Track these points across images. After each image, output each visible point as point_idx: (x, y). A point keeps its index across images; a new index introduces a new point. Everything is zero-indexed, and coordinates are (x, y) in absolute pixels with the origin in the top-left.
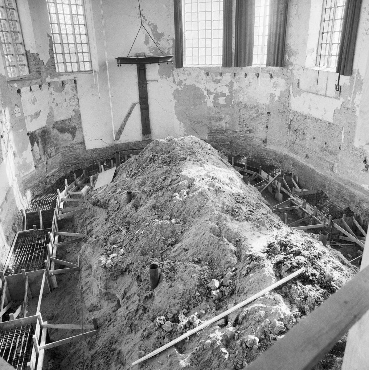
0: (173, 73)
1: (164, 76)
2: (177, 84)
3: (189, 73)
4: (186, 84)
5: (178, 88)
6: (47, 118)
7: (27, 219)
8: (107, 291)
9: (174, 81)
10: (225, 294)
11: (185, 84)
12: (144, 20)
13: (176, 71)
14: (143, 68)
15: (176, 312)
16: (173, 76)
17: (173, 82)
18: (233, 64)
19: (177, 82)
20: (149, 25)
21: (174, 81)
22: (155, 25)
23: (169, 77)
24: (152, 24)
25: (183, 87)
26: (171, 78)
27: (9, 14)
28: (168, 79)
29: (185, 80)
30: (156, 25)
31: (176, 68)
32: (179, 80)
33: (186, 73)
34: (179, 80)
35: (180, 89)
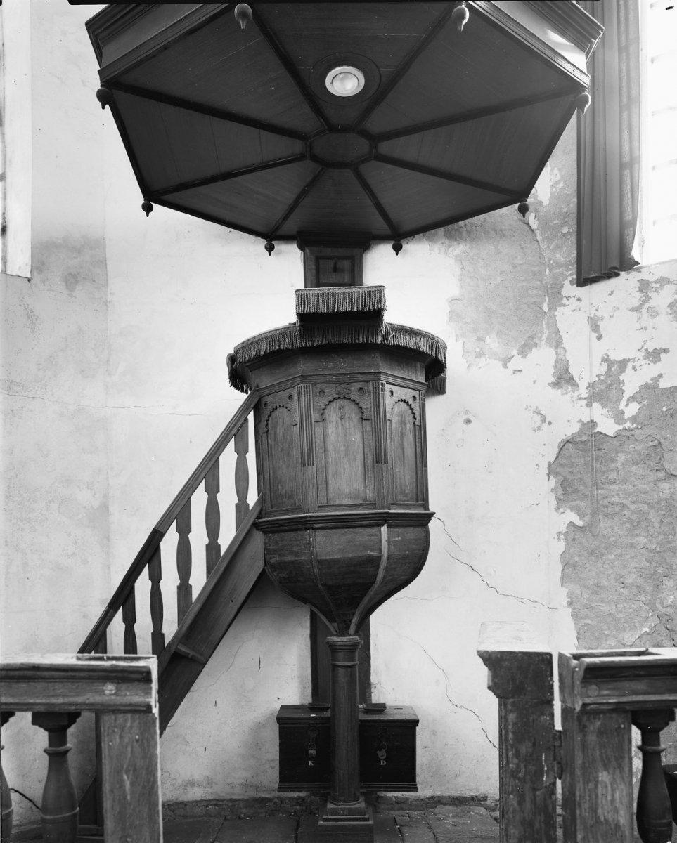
1: (493, 343)
2: (583, 391)
4: (663, 384)
5: (592, 424)
7: (551, 687)
8: (547, 422)
9: (563, 379)
10: (275, 434)
15: (421, 552)
16: (557, 343)
17: (556, 385)
18: (101, 838)
21: (563, 379)
23: (524, 350)
25: (632, 410)
26: (543, 359)
27: (609, 798)
28: (517, 362)
29: (655, 356)
32: (606, 360)
34: (606, 360)
35: (608, 426)
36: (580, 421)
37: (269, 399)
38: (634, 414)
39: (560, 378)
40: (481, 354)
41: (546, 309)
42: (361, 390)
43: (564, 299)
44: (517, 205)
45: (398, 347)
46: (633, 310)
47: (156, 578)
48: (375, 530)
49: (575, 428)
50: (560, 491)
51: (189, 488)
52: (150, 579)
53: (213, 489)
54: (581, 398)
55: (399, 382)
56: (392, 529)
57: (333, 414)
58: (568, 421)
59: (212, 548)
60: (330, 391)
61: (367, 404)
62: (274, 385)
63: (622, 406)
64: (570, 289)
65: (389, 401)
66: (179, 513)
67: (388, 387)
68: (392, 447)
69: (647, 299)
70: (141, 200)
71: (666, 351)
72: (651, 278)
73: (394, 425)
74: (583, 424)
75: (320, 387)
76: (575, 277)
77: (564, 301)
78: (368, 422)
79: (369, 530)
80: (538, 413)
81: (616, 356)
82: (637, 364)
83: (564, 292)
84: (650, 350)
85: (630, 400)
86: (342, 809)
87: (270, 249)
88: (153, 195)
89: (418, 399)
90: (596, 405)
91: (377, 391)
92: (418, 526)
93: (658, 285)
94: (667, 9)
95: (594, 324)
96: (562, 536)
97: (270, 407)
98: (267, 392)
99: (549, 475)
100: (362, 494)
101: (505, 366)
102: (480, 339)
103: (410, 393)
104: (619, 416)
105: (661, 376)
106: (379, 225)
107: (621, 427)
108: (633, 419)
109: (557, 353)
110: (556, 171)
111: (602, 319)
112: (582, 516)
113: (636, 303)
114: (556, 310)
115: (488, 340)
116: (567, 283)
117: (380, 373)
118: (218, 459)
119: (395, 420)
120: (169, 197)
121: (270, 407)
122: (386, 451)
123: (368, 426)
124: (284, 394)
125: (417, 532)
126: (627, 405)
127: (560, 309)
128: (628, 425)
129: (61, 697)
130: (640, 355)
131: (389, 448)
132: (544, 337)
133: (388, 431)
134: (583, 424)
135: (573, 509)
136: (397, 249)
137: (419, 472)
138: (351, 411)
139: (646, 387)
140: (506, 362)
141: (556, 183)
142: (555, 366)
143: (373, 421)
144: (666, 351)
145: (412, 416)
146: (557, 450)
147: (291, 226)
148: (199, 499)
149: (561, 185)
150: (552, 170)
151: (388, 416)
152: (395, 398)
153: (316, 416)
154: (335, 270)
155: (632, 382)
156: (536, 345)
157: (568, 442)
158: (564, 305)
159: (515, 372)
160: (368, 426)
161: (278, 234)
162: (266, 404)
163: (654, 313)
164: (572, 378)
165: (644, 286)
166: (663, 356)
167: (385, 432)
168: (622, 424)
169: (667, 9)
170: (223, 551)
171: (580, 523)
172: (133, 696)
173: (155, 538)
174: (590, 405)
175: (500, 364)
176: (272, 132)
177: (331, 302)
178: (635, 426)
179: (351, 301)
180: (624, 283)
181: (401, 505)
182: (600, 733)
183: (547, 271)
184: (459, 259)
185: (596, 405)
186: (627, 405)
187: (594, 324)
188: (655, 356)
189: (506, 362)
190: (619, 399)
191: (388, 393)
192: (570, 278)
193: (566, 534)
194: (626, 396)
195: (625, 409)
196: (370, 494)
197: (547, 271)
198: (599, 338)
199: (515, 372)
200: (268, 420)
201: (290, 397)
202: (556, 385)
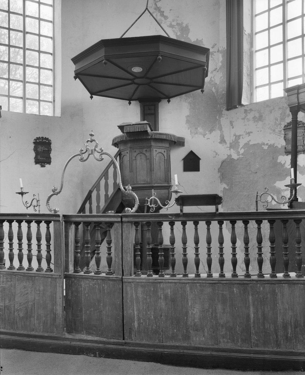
0: (220, 123)
1: (200, 130)
2: (228, 145)
3: (257, 115)
4: (251, 143)
5: (231, 155)
6: (33, 154)
9: (223, 141)
11: (247, 145)
12: (163, 19)
13: (227, 117)
14: (153, 112)
16: (221, 129)
17: (220, 143)
19: (228, 143)
20: (171, 26)
21: (223, 141)
22: (184, 25)
23: (211, 131)
24: (178, 24)
25: (242, 151)
26: (216, 134)
29: (249, 133)
30: (187, 26)
31: (228, 109)
33: (250, 116)
35: (235, 157)
36: (227, 155)
37: (122, 153)
38: (243, 152)
39: (221, 141)
40: (197, 133)
41: (218, 118)
42: (146, 151)
43: (223, 115)
44: (200, 90)
45: (155, 138)
46: (242, 119)
47: (91, 204)
48: (150, 190)
49: (226, 157)
50: (221, 177)
51: (100, 179)
52: (89, 204)
53: (107, 179)
54: (227, 147)
55: (158, 147)
56: (155, 190)
57: (138, 158)
58: (224, 155)
59: (106, 195)
60: (138, 151)
61: (148, 154)
62: (123, 149)
63: (239, 150)
64: (225, 112)
65: (155, 153)
66: (97, 186)
67: (155, 149)
68: (156, 166)
69: (247, 115)
70: (90, 95)
71: (252, 132)
72: (248, 109)
73: (157, 160)
74: (228, 156)
75: (134, 150)
76: (226, 108)
77: (223, 116)
78: (148, 160)
79: (148, 191)
80: (215, 152)
81: (238, 134)
82: (244, 137)
83: (223, 113)
84: (247, 132)
85: (241, 148)
86: (144, 272)
87: (130, 103)
88: (93, 93)
89: (166, 151)
90: (232, 150)
91: (150, 151)
92: (166, 189)
93: (250, 111)
94: (16, 193)
95: (231, 123)
96: (222, 192)
97: (123, 155)
98: (122, 151)
99: (218, 172)
100: (146, 180)
101: (204, 137)
102: (196, 129)
103: (162, 151)
104: (238, 153)
105: (250, 140)
106: (162, 96)
107: (239, 157)
108: (242, 154)
109: (221, 132)
110: (221, 73)
111: (234, 122)
112: (228, 185)
113: (243, 117)
114: (220, 118)
115: (199, 129)
116: (224, 110)
117: (151, 146)
118: (108, 170)
119: (157, 158)
120: (99, 94)
121: (123, 155)
122: (154, 167)
123: (148, 161)
124: (126, 152)
125: (166, 191)
126: (241, 150)
127: (222, 118)
128: (241, 156)
129: (48, 219)
130: (244, 134)
131: (155, 167)
132: (217, 127)
133: (154, 162)
134: (228, 156)
135: (225, 183)
136: (169, 101)
137: (166, 174)
138: (143, 156)
139: (246, 144)
140: (204, 136)
141: (221, 77)
142: (220, 137)
143: (150, 160)
144: (252, 132)
145: (163, 157)
146: (220, 164)
147: (135, 96)
148: (103, 182)
149: (222, 78)
150: (220, 73)
151: (154, 158)
152: (157, 152)
153: (134, 158)
154: (149, 109)
155: (242, 142)
156: (214, 130)
157: (224, 161)
158: (223, 117)
159: (207, 139)
160: (148, 161)
161: (132, 99)
162: (122, 154)
163: (248, 120)
164: (225, 141)
165: (246, 111)
166: (251, 134)
167: (153, 163)
168: (239, 156)
169: (16, 193)
170: (109, 196)
171: (227, 188)
172: (57, 219)
173: (90, 192)
174: (230, 150)
175: (202, 136)
176: (109, 90)
177: (133, 129)
178: (243, 156)
179: (138, 129)
180: (240, 110)
181: (159, 183)
182: (126, 226)
183: (218, 106)
184: (190, 103)
185: (232, 150)
186: (241, 150)
187: (231, 123)
188: (249, 133)
189: (204, 136)
190: (238, 148)
191: (154, 151)
192: (225, 108)
193: (223, 191)
194: (241, 146)
195: (240, 151)
196: (149, 180)
197: (218, 106)
198: (233, 128)
199: (207, 139)
200: (122, 159)
201: (127, 153)
202: (220, 143)
